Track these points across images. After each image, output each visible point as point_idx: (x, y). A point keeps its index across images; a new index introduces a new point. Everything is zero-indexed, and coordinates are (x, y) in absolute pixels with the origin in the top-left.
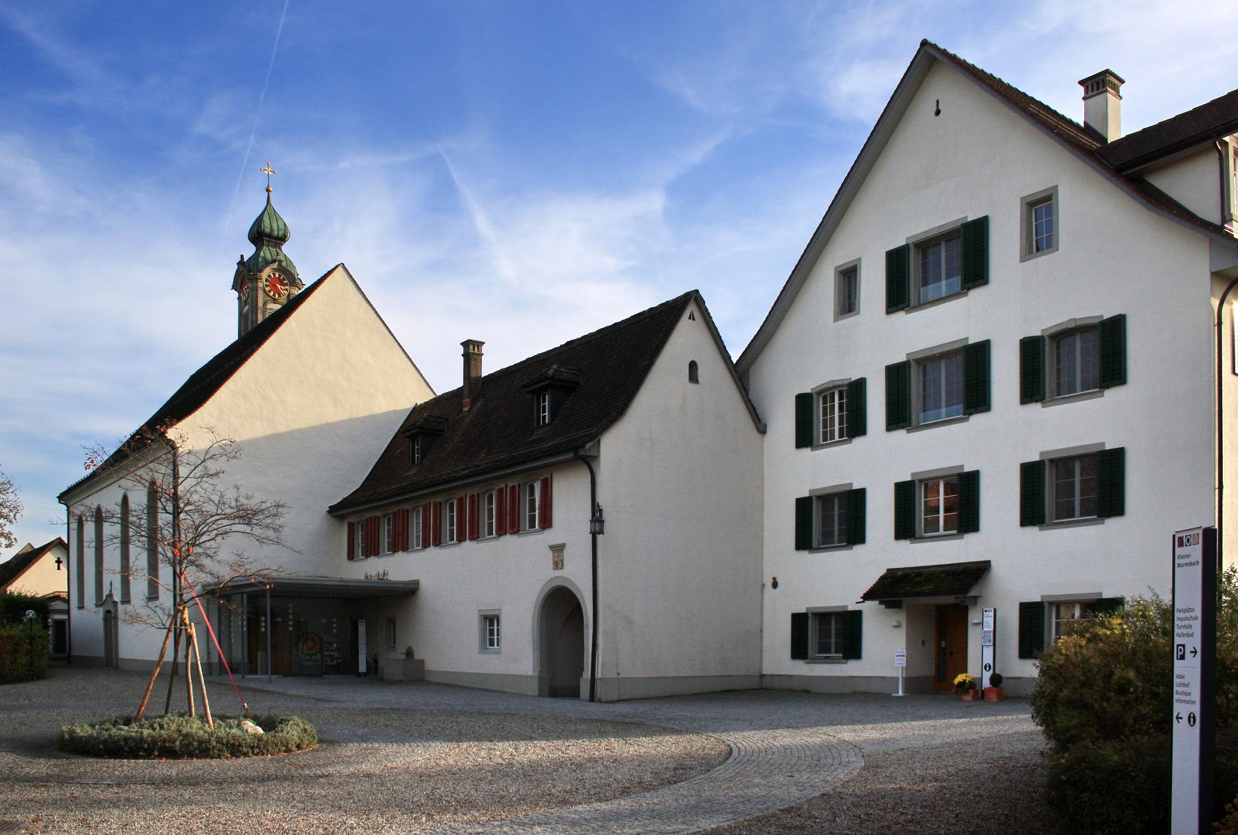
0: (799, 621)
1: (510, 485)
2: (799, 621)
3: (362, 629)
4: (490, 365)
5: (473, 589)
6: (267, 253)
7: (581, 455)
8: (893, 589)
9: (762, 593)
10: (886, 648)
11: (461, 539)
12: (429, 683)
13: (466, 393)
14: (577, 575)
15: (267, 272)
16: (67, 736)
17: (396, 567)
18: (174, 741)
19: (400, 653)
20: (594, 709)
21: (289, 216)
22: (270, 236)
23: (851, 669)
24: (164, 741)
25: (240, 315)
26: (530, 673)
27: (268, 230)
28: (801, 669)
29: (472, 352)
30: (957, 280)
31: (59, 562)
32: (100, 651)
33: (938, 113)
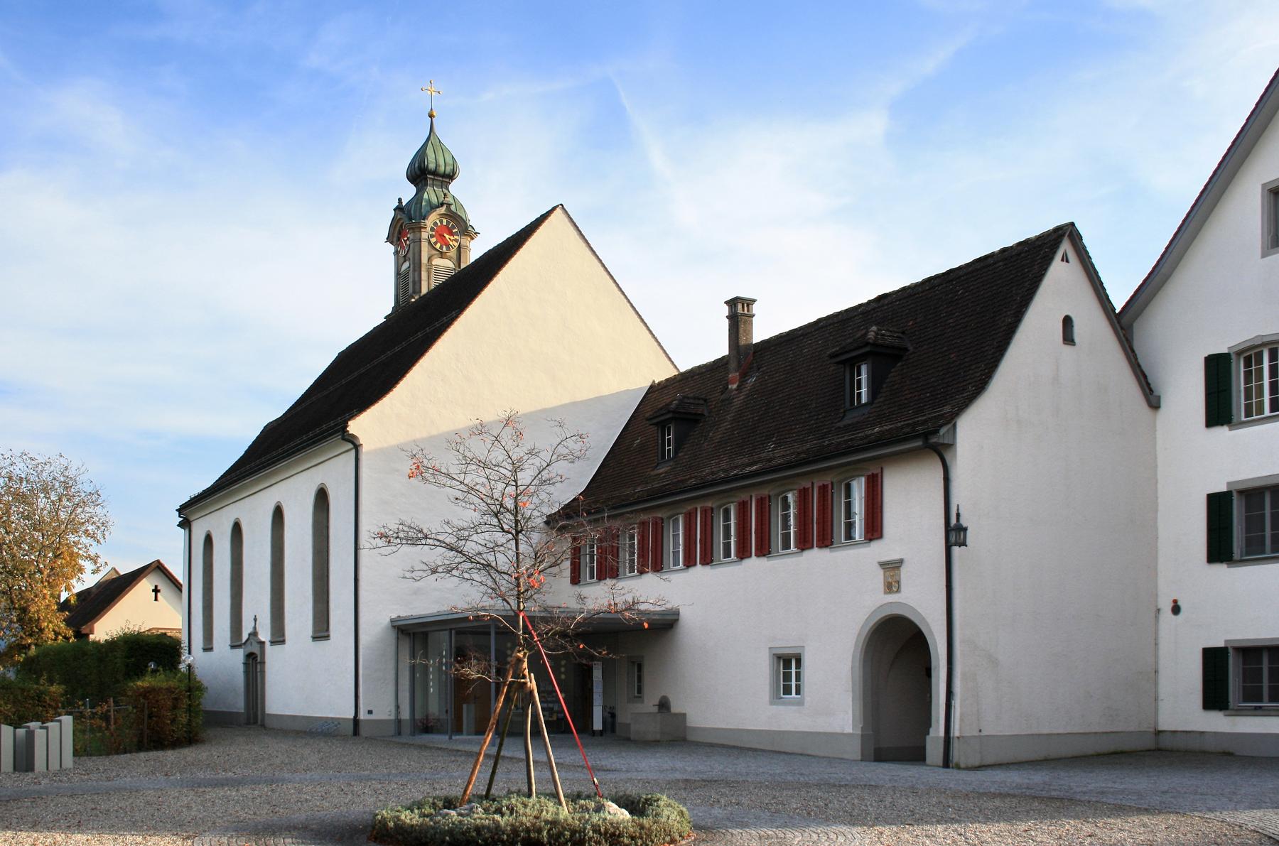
0: (1214, 660)
1: (818, 483)
2: (1214, 660)
3: (597, 674)
4: (763, 329)
5: (760, 624)
6: (431, 194)
7: (927, 437)
9: (1157, 618)
11: (743, 553)
12: (698, 745)
13: (733, 365)
14: (921, 600)
15: (432, 219)
16: (391, 824)
17: (645, 592)
18: (539, 831)
19: (650, 704)
20: (951, 778)
21: (457, 143)
22: (435, 173)
24: (528, 830)
25: (398, 274)
26: (849, 730)
27: (432, 166)
28: (1218, 722)
29: (739, 312)
31: (156, 591)
32: (239, 705)
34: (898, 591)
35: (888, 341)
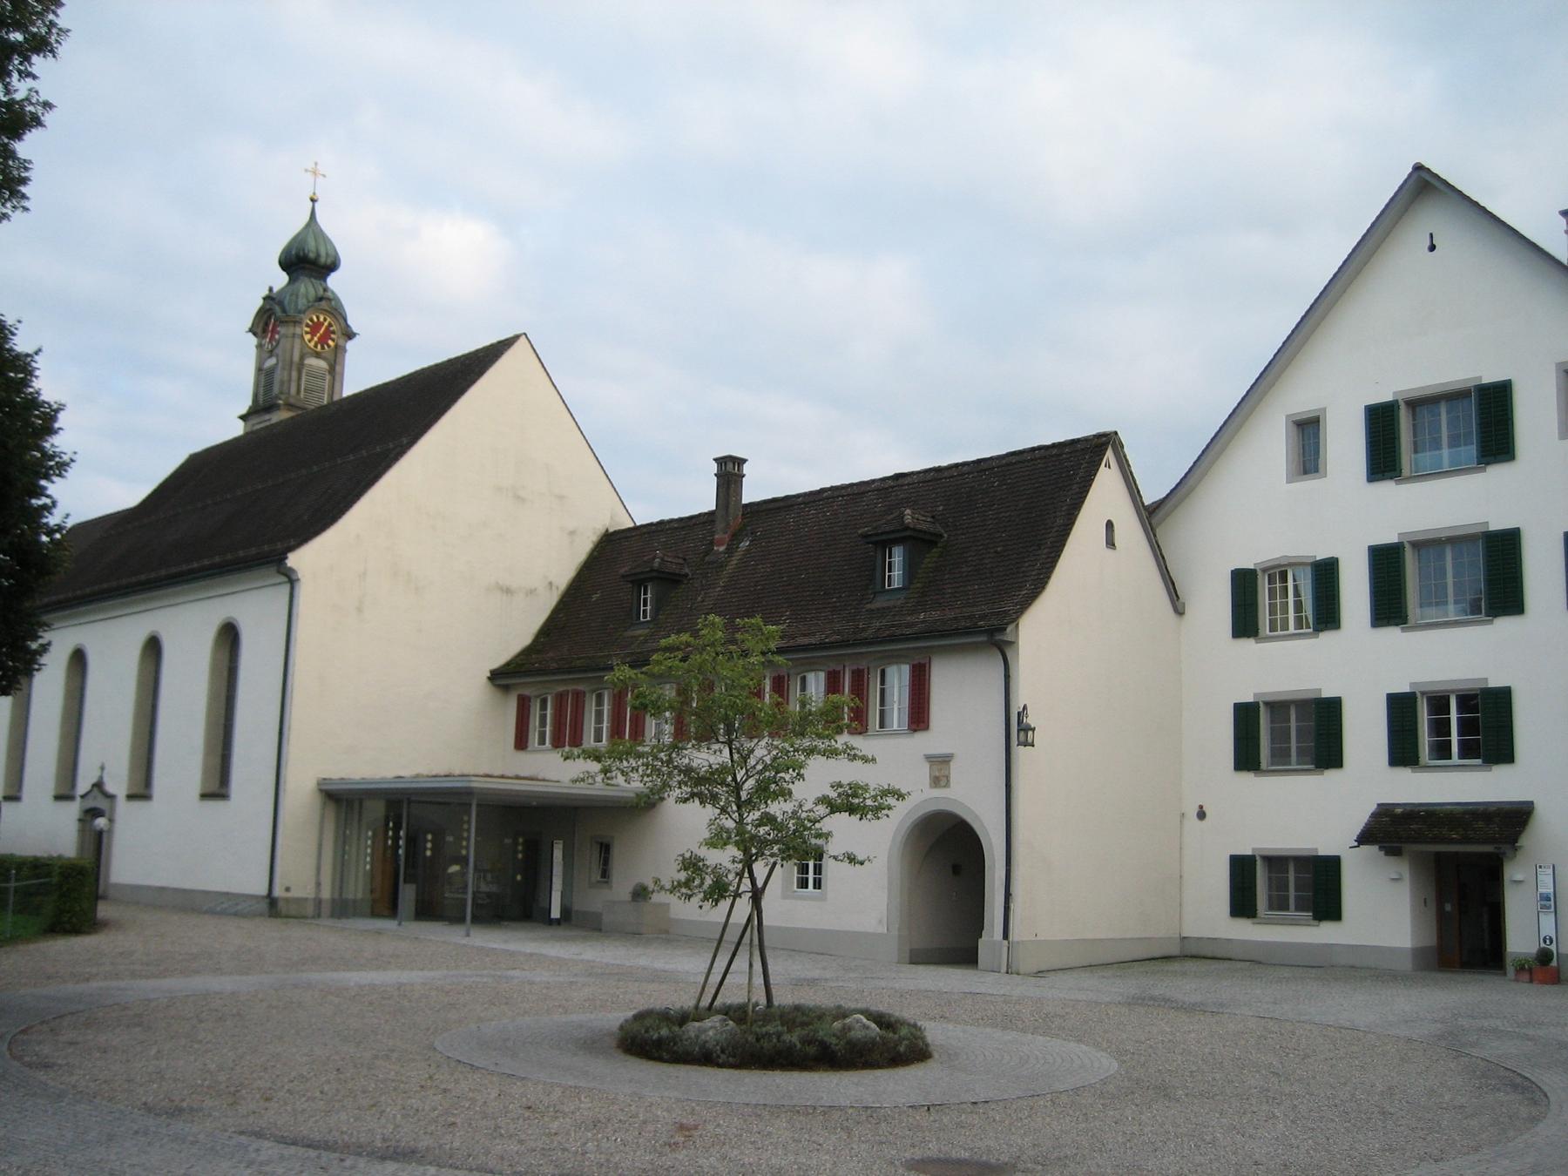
0: (1242, 868)
2: (1242, 868)
4: (753, 491)
6: (306, 287)
7: (990, 633)
8: (1390, 830)
10: (1383, 908)
23: (1324, 934)
25: (259, 370)
29: (730, 472)
30: (1472, 450)
33: (1432, 248)
34: (947, 785)
35: (924, 527)
